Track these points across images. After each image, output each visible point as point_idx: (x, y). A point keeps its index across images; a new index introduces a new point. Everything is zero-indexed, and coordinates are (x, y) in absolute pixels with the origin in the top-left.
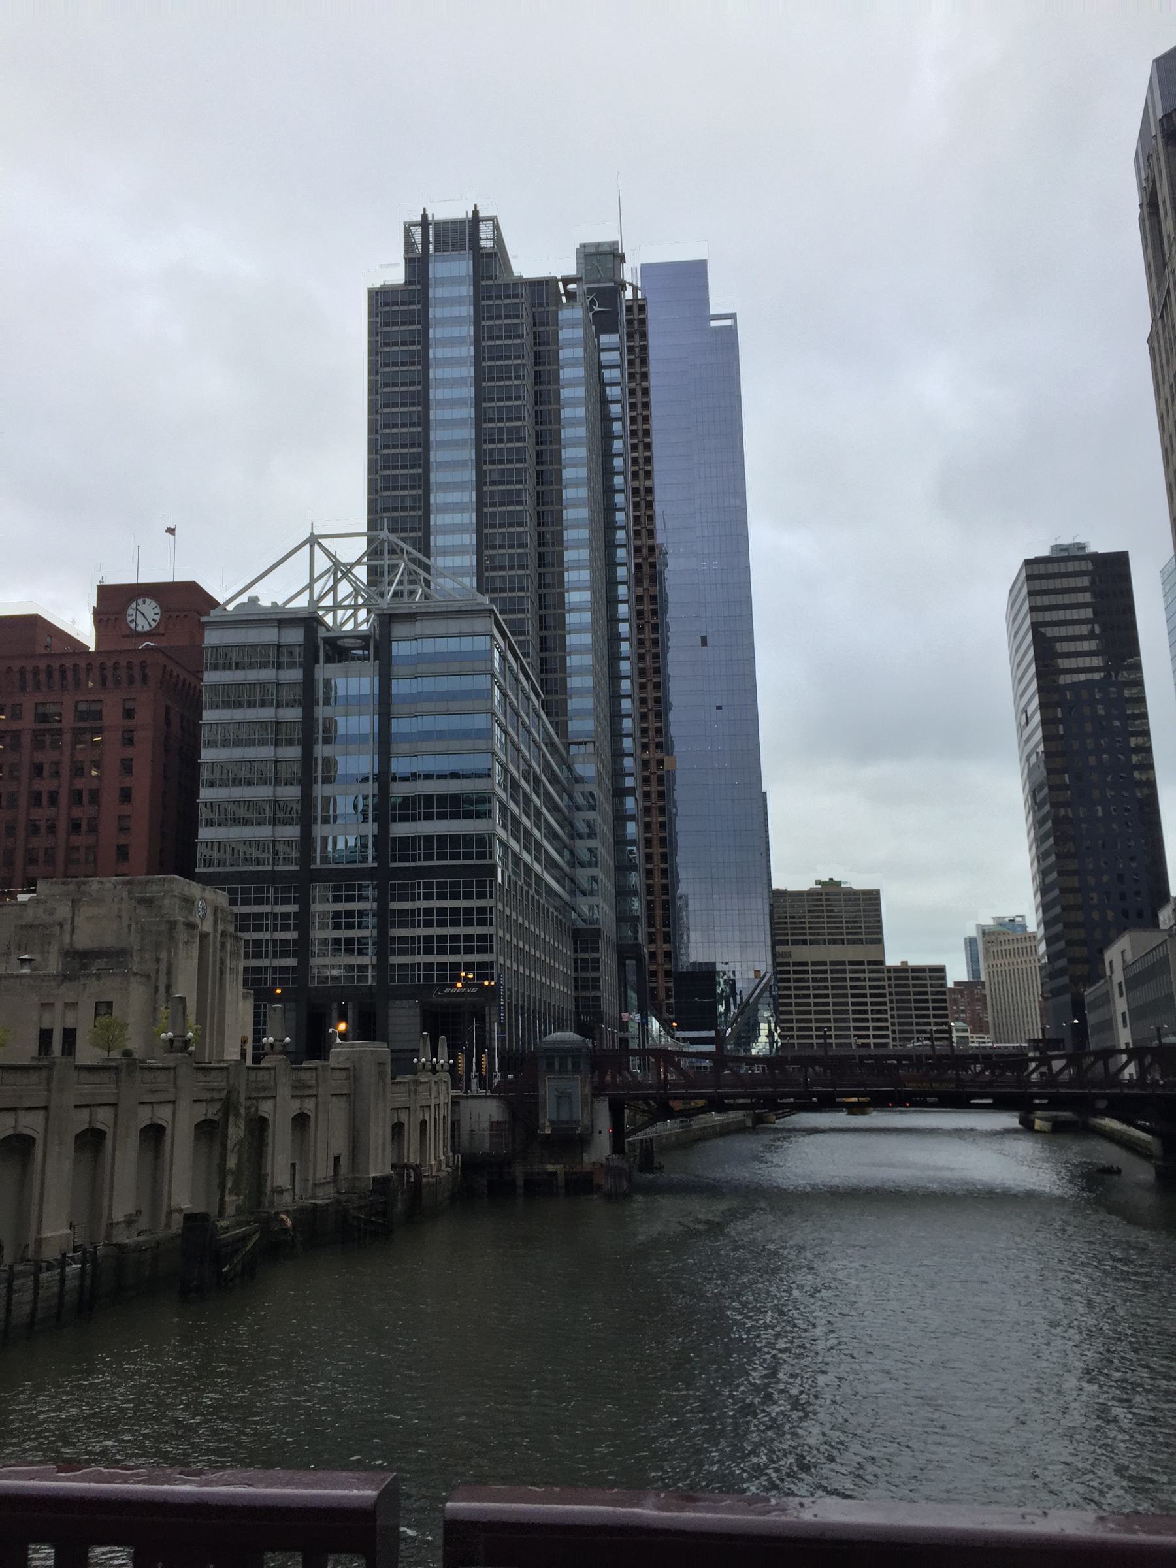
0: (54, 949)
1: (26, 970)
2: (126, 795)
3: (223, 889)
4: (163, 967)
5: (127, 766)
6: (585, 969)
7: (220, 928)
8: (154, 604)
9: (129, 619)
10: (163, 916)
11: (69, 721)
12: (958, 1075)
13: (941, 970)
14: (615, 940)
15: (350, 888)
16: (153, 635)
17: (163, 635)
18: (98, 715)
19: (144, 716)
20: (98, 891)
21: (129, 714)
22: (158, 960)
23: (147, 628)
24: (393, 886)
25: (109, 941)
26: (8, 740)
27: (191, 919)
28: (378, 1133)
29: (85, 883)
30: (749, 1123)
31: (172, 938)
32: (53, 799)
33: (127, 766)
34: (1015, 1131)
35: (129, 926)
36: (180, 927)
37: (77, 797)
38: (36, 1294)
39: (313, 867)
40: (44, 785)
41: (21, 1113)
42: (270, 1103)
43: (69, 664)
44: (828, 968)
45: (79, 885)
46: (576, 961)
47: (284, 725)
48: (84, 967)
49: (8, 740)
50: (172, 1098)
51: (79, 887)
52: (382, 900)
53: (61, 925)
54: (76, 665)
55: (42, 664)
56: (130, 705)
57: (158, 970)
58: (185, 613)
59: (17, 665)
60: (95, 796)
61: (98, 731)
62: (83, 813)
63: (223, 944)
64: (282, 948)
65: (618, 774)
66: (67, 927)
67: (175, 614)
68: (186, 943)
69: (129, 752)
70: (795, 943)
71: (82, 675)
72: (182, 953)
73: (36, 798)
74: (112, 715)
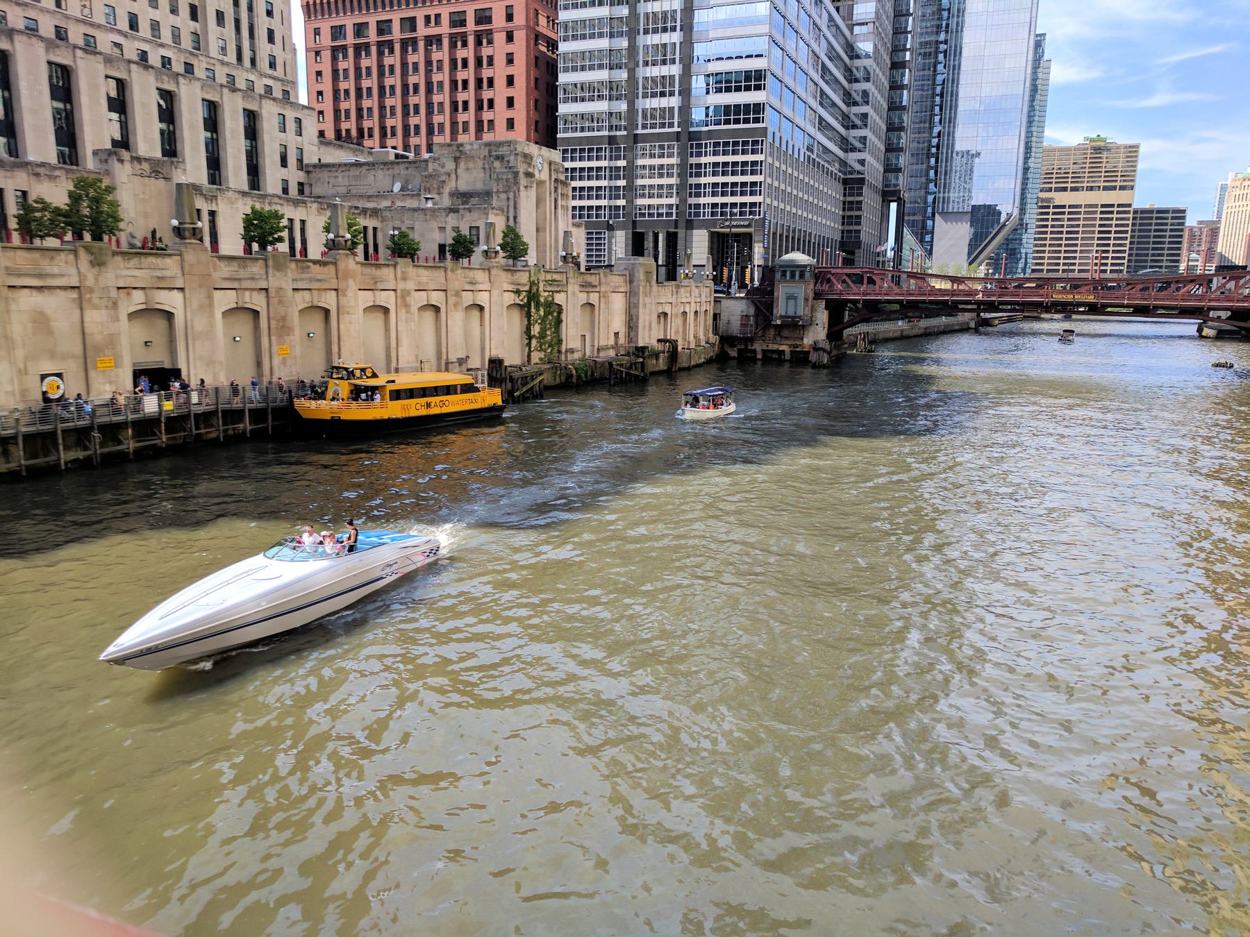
1: (430, 204)
4: (512, 203)
6: (851, 209)
13: (1180, 214)
14: (880, 186)
15: (699, 146)
21: (510, 18)
22: (508, 199)
25: (479, 186)
27: (530, 170)
28: (646, 316)
30: (972, 325)
31: (516, 183)
34: (1191, 338)
41: (377, 293)
42: (563, 295)
44: (1115, 209)
46: (844, 203)
52: (683, 155)
53: (449, 175)
60: (491, 82)
63: (556, 189)
64: (614, 192)
65: (897, 49)
66: (453, 176)
70: (1057, 190)
72: (523, 193)
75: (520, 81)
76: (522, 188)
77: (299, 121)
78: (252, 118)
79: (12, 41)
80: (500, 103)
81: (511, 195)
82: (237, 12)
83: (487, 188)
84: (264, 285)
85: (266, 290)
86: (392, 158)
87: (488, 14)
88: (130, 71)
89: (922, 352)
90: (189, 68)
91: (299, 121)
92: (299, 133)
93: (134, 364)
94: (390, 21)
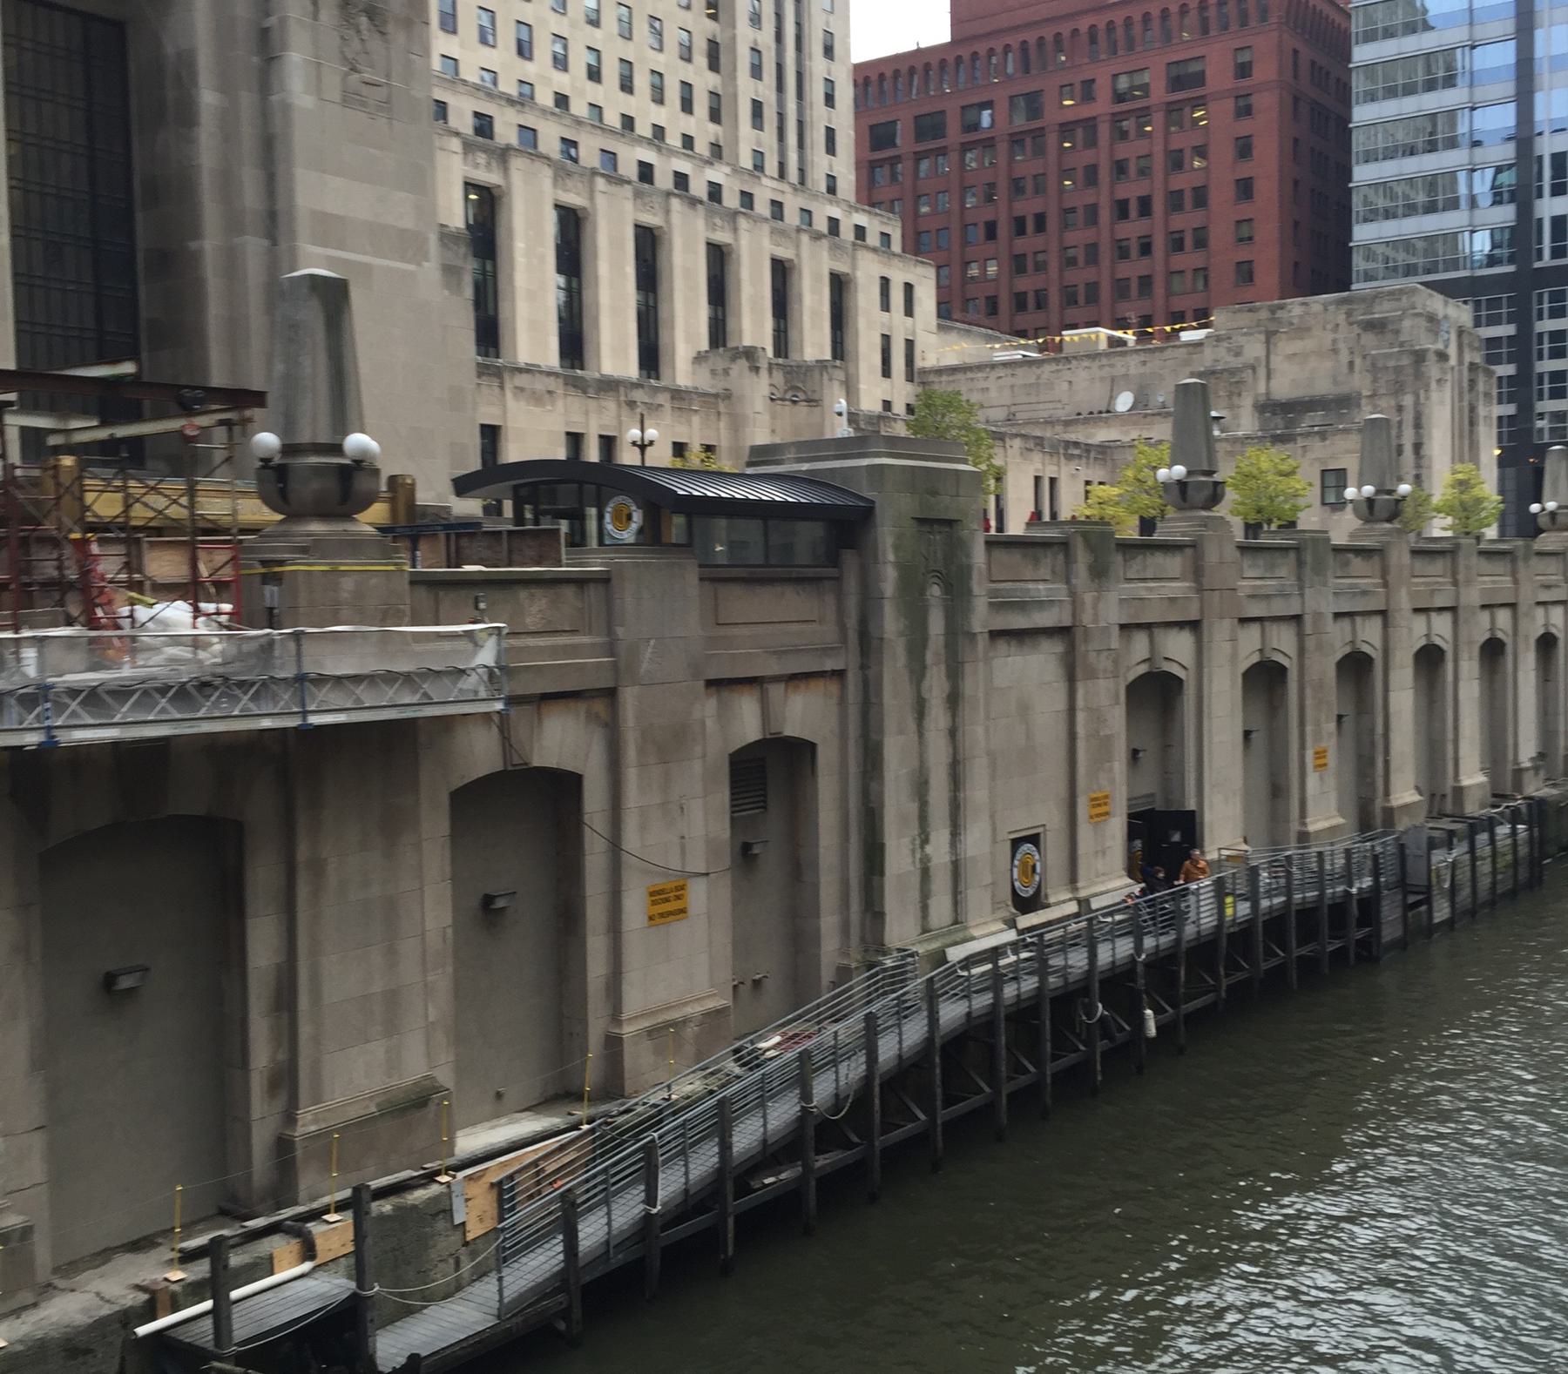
0: (1247, 403)
2: (1245, 189)
3: (1465, 302)
4: (1409, 417)
5: (1244, 148)
7: (1467, 358)
11: (1159, 93)
12: (195, 654)
18: (1199, 79)
19: (1266, 70)
20: (1301, 317)
21: (1244, 70)
22: (1400, 409)
24: (1540, 296)
25: (1323, 387)
26: (1080, 133)
29: (1281, 307)
31: (1418, 375)
32: (1145, 205)
35: (1351, 364)
36: (1432, 357)
37: (1175, 201)
38: (1494, 863)
39: (1537, 265)
40: (1131, 190)
43: (982, 51)
45: (1273, 310)
47: (1459, 51)
48: (1291, 424)
49: (1080, 133)
50: (1193, 615)
51: (1273, 312)
53: (1254, 369)
56: (1244, 57)
57: (1400, 423)
59: (1014, 40)
60: (1201, 197)
62: (1186, 221)
66: (1262, 372)
68: (1439, 381)
69: (1244, 127)
72: (1434, 396)
73: (1122, 209)
74: (1219, 76)
75: (1268, 188)
76: (1433, 385)
77: (909, 288)
78: (840, 286)
79: (506, 170)
80: (1221, 235)
81: (1408, 400)
82: (781, 103)
84: (1294, 610)
85: (1297, 619)
86: (1103, 345)
87: (1195, 67)
88: (667, 212)
89: (642, 766)
90: (747, 199)
91: (909, 288)
92: (909, 311)
94: (943, 112)
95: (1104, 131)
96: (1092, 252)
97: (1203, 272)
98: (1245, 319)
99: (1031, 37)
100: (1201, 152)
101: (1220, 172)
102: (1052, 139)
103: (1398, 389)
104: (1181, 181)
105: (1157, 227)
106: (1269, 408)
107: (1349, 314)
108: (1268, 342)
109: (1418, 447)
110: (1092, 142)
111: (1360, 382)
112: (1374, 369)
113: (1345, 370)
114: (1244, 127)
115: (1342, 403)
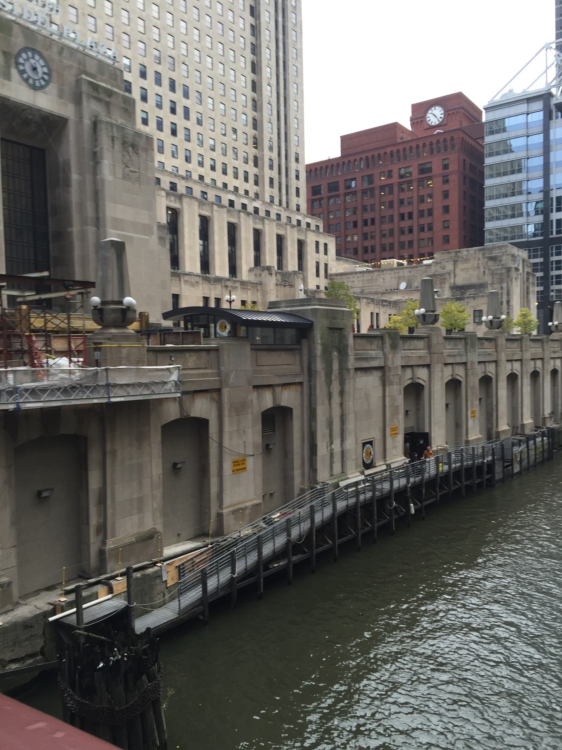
0: (447, 286)
2: (446, 209)
3: (525, 250)
4: (505, 291)
5: (446, 195)
7: (526, 270)
8: (440, 109)
9: (428, 119)
10: (502, 265)
11: (416, 175)
16: (442, 126)
17: (446, 125)
18: (430, 170)
19: (454, 167)
21: (446, 167)
22: (502, 288)
23: (437, 123)
25: (474, 281)
29: (459, 252)
31: (508, 276)
32: (410, 215)
33: (446, 195)
35: (484, 272)
38: (535, 451)
39: (551, 237)
40: (405, 210)
43: (352, 160)
45: (456, 253)
47: (523, 160)
48: (463, 294)
53: (449, 274)
54: (418, 145)
55: (401, 148)
56: (446, 162)
57: (502, 293)
58: (457, 111)
60: (430, 212)
61: (430, 178)
62: (425, 221)
66: (452, 275)
67: (451, 112)
68: (516, 278)
69: (446, 187)
71: (421, 149)
72: (514, 284)
73: (402, 217)
74: (437, 169)
75: (454, 209)
76: (514, 280)
77: (326, 245)
78: (301, 244)
79: (181, 203)
80: (438, 226)
81: (505, 285)
82: (280, 178)
83: (481, 281)
86: (395, 265)
88: (239, 218)
91: (326, 245)
93: (405, 431)
95: (396, 188)
96: (391, 232)
97: (431, 239)
98: (446, 256)
99: (369, 155)
100: (430, 196)
101: (438, 203)
102: (377, 191)
103: (501, 281)
104: (423, 207)
105: (415, 223)
106: (455, 288)
107: (483, 254)
108: (454, 264)
109: (508, 302)
110: (391, 192)
111: (488, 279)
112: (493, 274)
113: (482, 274)
114: (446, 187)
115: (481, 286)
